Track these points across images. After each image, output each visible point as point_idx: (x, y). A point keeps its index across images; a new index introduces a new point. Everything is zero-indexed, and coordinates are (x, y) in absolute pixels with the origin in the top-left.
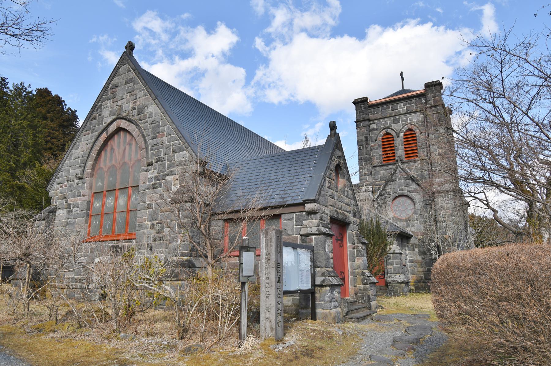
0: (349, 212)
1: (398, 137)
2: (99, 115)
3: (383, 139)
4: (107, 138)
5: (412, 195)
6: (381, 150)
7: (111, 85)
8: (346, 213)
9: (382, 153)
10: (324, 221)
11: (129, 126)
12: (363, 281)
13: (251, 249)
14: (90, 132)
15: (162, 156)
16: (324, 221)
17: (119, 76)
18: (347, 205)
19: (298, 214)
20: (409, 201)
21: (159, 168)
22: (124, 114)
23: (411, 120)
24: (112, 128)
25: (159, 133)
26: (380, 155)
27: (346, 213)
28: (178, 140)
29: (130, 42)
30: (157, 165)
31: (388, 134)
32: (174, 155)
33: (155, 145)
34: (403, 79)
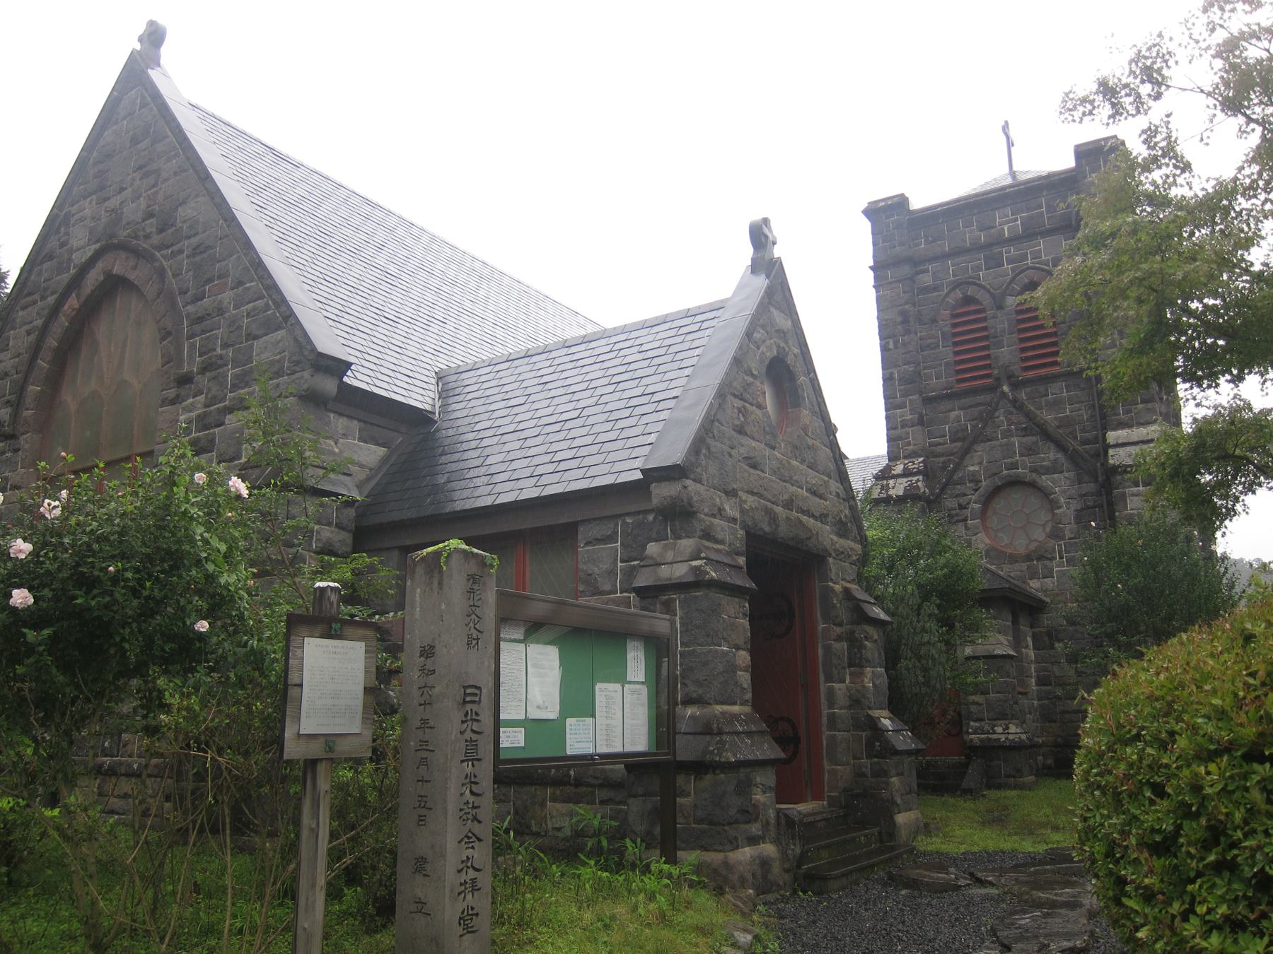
0: (822, 518)
1: (1000, 307)
2: (62, 245)
3: (954, 316)
4: (79, 311)
5: (1045, 480)
6: (950, 349)
7: (95, 154)
8: (810, 522)
9: (950, 358)
10: (722, 542)
11: (134, 268)
12: (870, 744)
13: (349, 630)
14: (37, 296)
15: (219, 351)
16: (722, 542)
17: (116, 123)
18: (814, 493)
19: (629, 520)
20: (1034, 501)
21: (209, 389)
22: (123, 234)
23: (1037, 255)
24: (94, 278)
25: (210, 280)
26: (947, 364)
27: (810, 522)
28: (261, 297)
29: (152, 23)
30: (203, 381)
31: (968, 300)
32: (251, 347)
33: (200, 320)
34: (1010, 144)
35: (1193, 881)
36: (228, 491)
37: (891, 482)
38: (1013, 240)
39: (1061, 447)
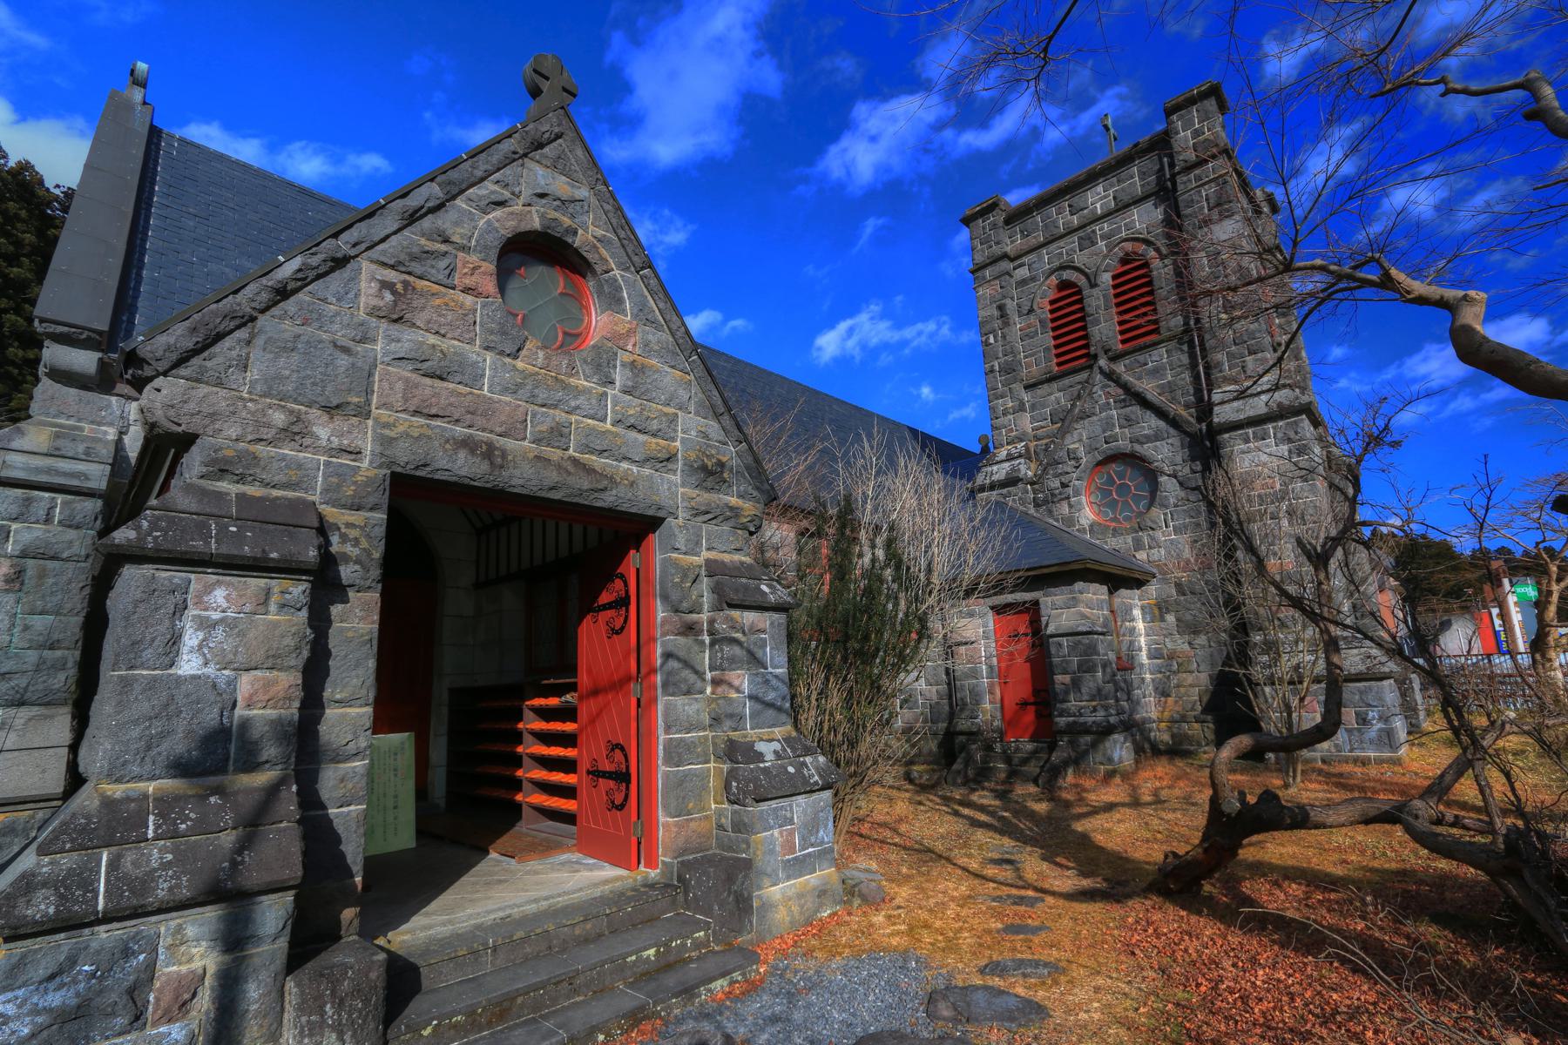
5: (1147, 450)
31: (1064, 285)
35: (848, 703)
36: (1229, 815)
37: (995, 468)
38: (1107, 215)
39: (1161, 413)
